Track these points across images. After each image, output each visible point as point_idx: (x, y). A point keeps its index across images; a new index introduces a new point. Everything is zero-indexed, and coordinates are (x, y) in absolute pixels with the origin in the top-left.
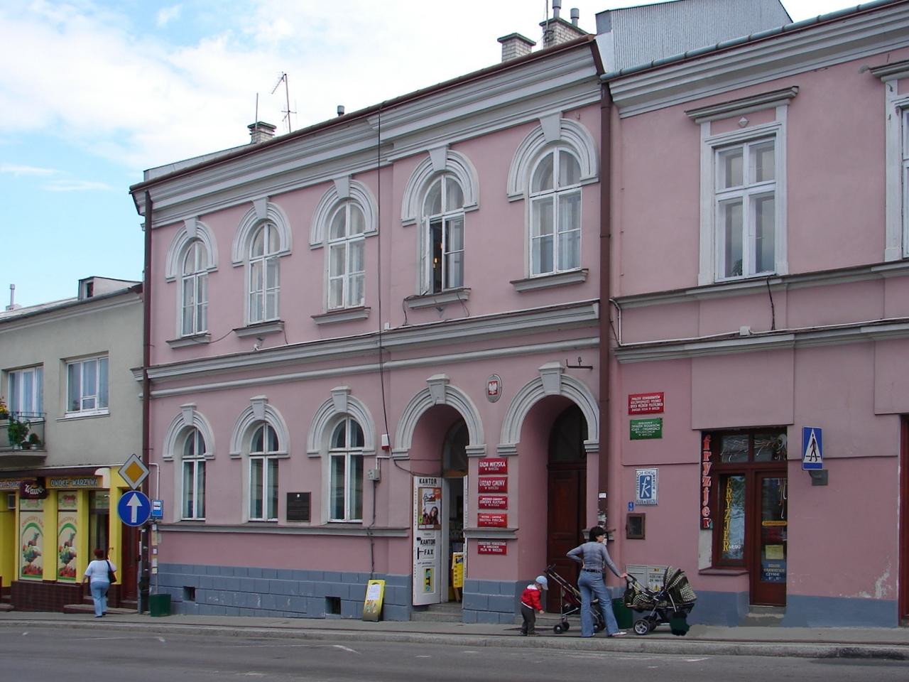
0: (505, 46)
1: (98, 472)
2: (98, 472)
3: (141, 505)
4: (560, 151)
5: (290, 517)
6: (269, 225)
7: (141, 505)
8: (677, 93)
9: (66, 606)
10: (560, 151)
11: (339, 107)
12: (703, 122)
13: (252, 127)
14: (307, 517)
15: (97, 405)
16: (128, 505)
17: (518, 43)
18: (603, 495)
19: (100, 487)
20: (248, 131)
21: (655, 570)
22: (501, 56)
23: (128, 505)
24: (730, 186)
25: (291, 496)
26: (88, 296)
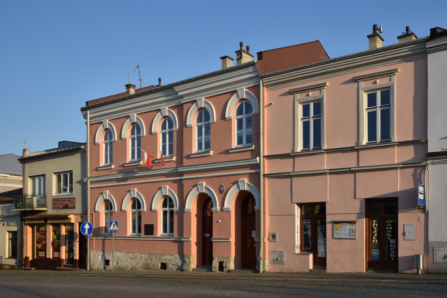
0: (223, 61)
1: (69, 217)
2: (69, 217)
3: (89, 227)
4: (245, 102)
5: (146, 234)
6: (136, 125)
7: (89, 227)
8: (288, 83)
9: (103, 257)
10: (245, 102)
11: (159, 78)
12: (295, 94)
13: (126, 86)
14: (152, 233)
15: (68, 191)
16: (84, 227)
17: (228, 59)
18: (207, 235)
19: (69, 222)
20: (125, 87)
21: (280, 253)
22: (221, 63)
23: (84, 227)
24: (88, 105)
25: (146, 226)
26: (198, 149)
